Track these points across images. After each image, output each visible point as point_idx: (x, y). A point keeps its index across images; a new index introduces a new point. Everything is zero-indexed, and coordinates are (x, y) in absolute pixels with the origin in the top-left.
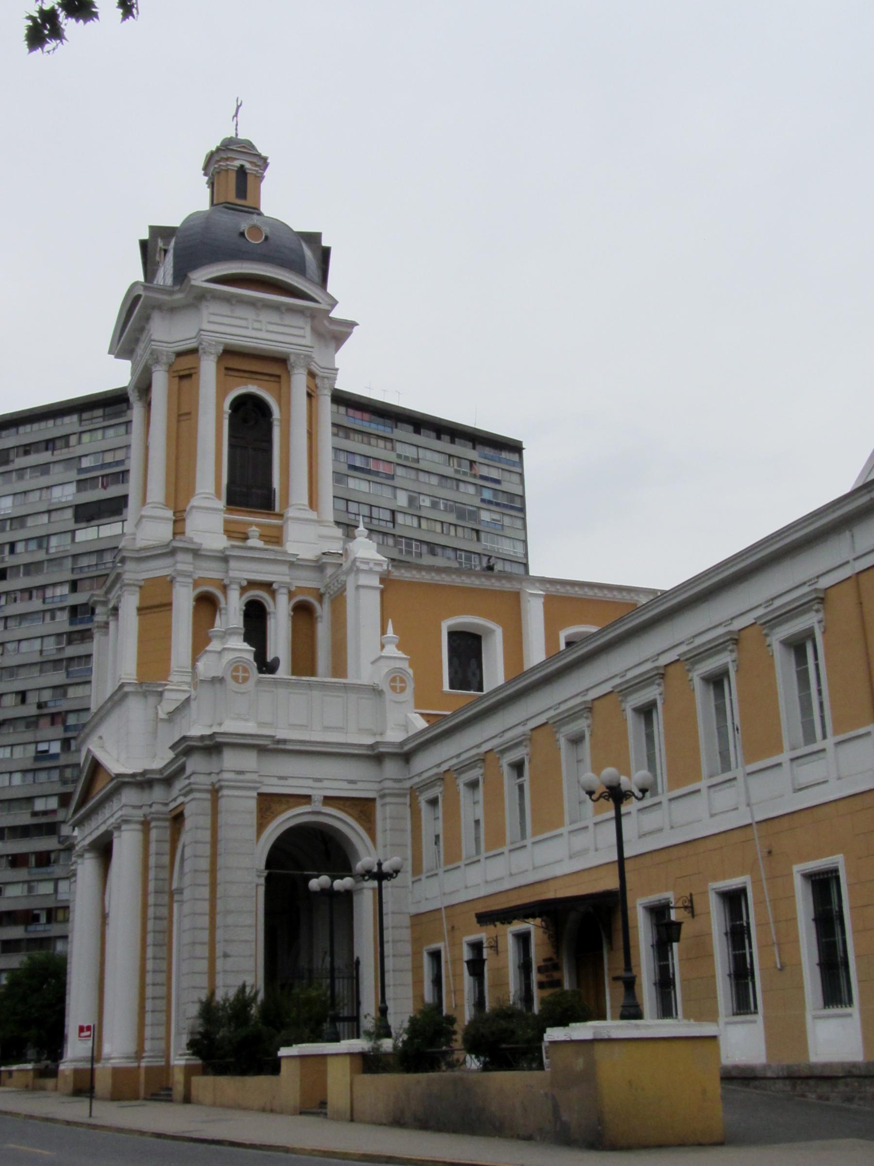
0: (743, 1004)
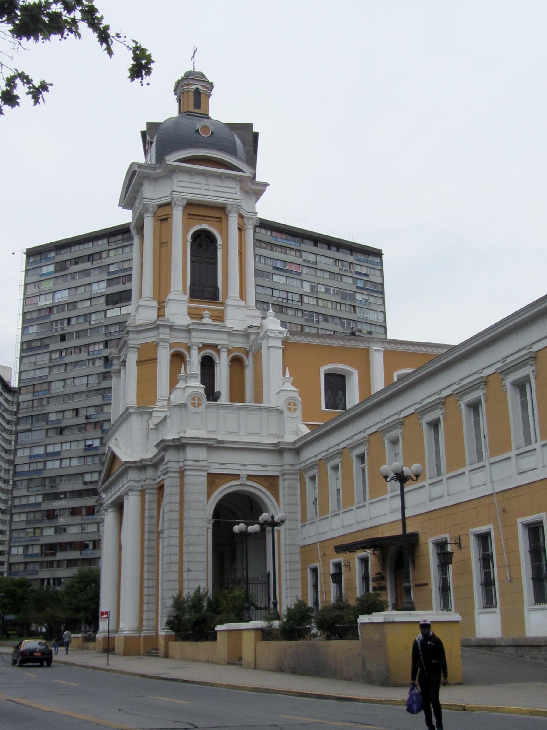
0: (489, 602)
